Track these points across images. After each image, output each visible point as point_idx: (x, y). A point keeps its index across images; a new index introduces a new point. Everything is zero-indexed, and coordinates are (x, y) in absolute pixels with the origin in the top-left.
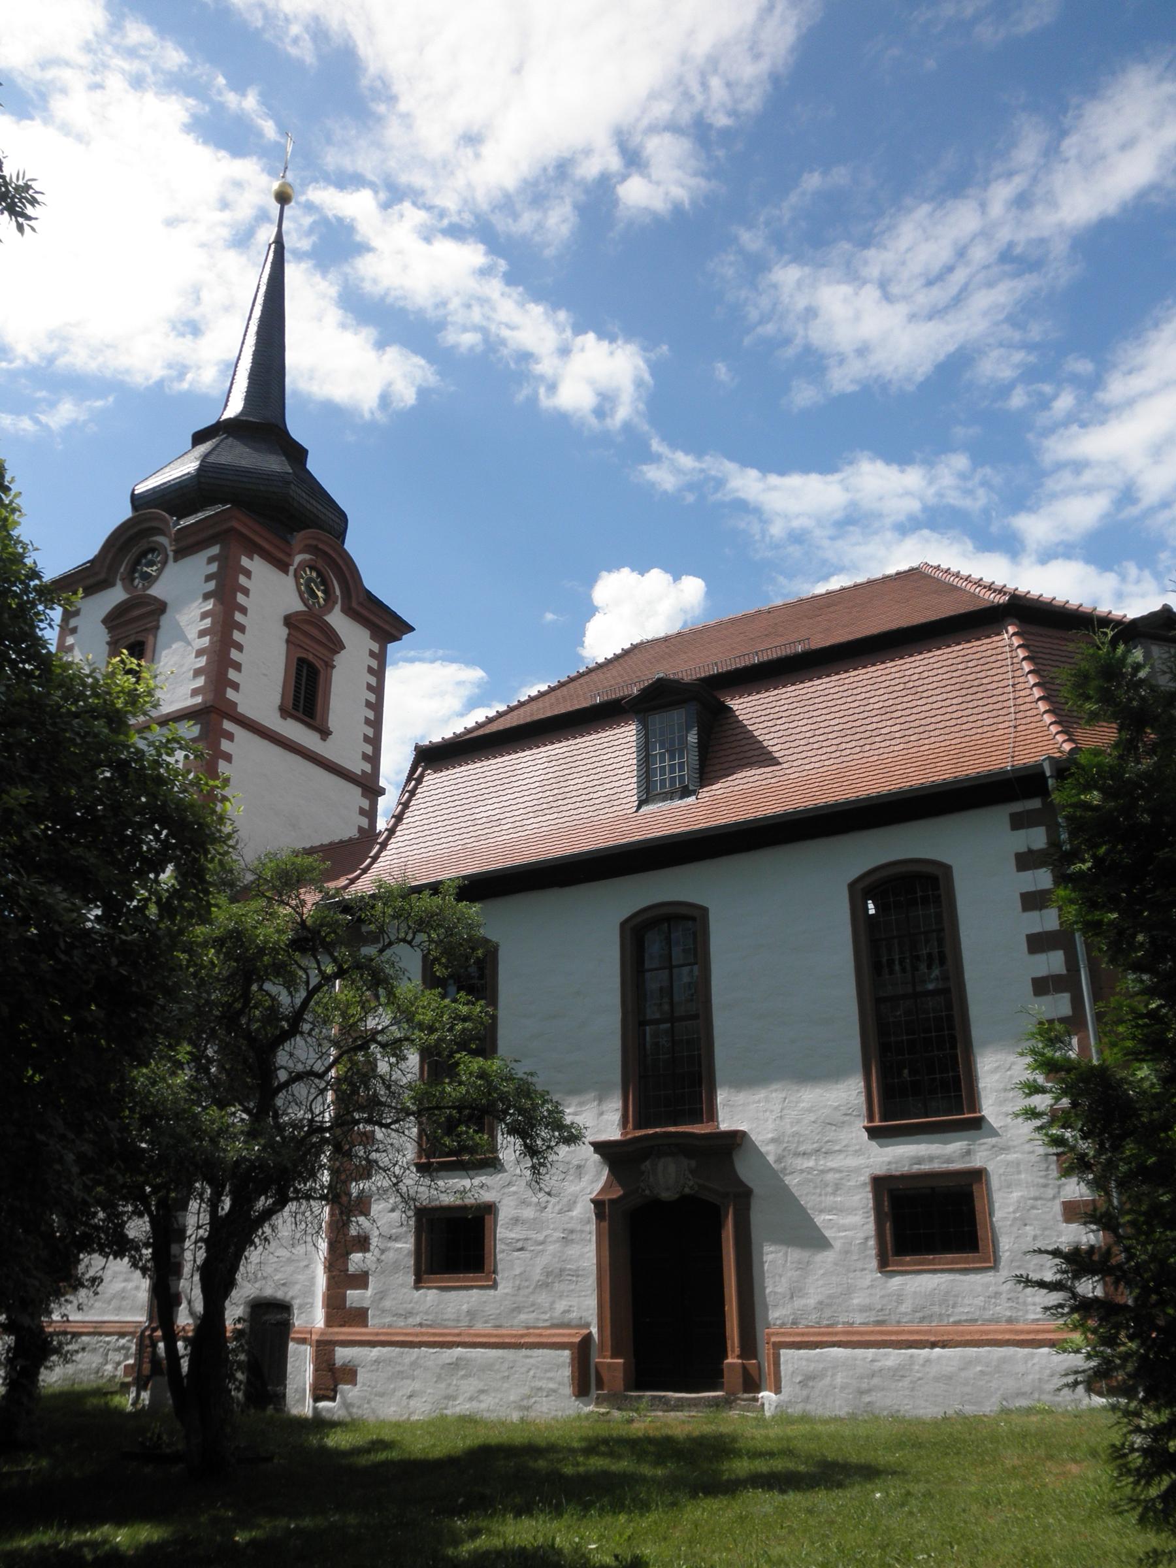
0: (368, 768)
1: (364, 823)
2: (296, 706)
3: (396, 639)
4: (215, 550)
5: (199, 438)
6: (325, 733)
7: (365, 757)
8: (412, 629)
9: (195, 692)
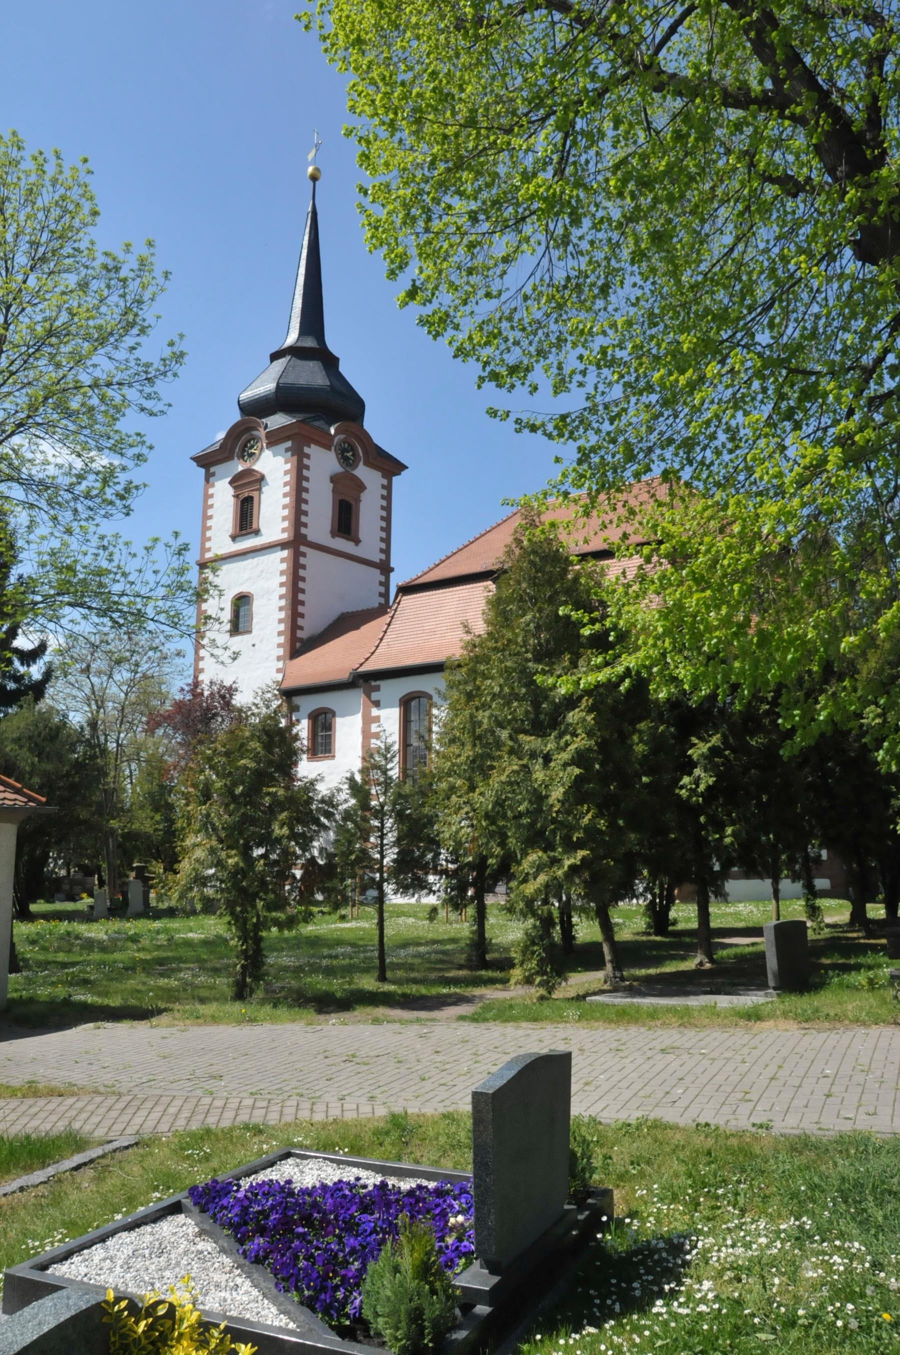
0: (383, 557)
1: (382, 601)
2: (340, 530)
3: (398, 474)
4: (289, 444)
5: (275, 357)
6: (357, 541)
7: (382, 551)
8: (404, 467)
9: (284, 530)
